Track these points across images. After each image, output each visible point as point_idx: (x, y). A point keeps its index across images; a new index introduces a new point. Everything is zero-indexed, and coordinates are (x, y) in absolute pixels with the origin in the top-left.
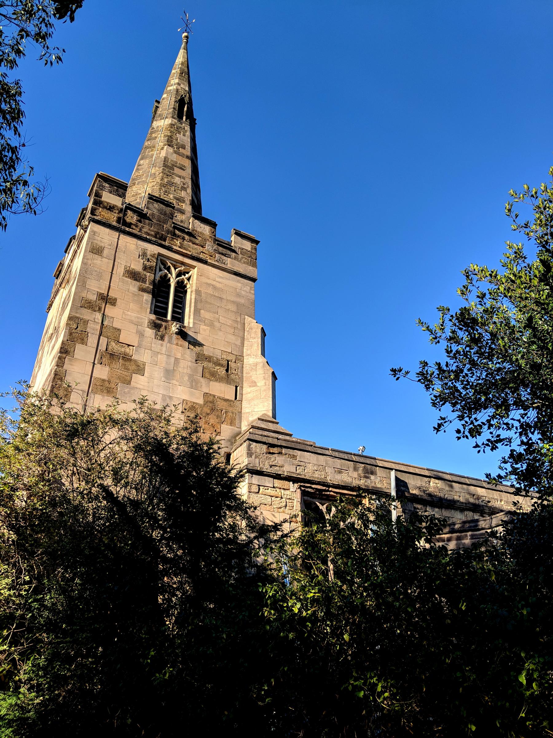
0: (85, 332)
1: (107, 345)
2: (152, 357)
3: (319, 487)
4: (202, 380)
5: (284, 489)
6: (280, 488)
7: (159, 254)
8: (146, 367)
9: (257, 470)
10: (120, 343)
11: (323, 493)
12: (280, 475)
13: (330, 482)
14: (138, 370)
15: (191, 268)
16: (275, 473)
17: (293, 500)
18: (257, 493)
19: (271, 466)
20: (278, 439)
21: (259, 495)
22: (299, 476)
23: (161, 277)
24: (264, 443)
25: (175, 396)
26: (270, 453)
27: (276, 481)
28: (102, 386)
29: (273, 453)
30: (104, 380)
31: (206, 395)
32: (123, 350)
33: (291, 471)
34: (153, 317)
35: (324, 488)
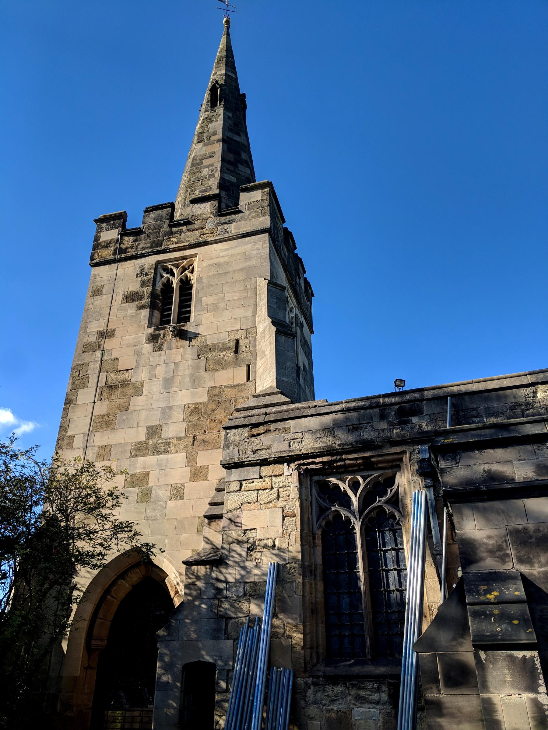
0: (87, 375)
1: (107, 379)
2: (150, 372)
3: (325, 459)
4: (205, 375)
5: (275, 476)
6: (270, 476)
7: (158, 263)
8: (144, 385)
9: (235, 463)
10: (119, 371)
11: (335, 464)
12: (266, 459)
13: (338, 448)
14: (137, 391)
15: (194, 257)
16: (259, 459)
17: (289, 486)
18: (238, 491)
19: (255, 452)
20: (266, 414)
21: (240, 494)
22: (291, 454)
23: (163, 284)
24: (245, 426)
25: (176, 404)
26: (253, 436)
27: (263, 468)
28: (101, 422)
29: (258, 435)
30: (103, 416)
31: (211, 390)
32: (122, 377)
33: (282, 450)
34: (151, 330)
35: (334, 458)
